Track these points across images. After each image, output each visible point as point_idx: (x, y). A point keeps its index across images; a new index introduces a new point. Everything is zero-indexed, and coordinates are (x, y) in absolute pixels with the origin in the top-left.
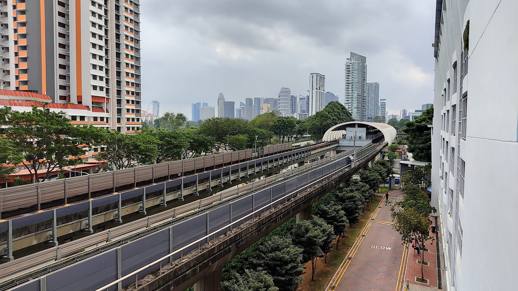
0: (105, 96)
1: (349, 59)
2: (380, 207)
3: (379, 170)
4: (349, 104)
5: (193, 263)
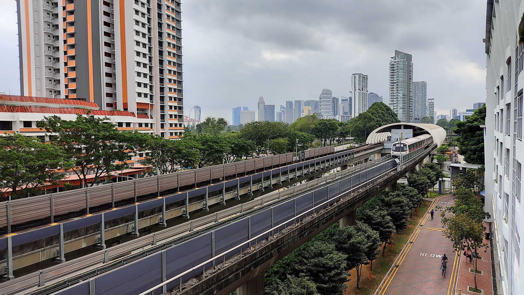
0: (149, 103)
1: (393, 58)
3: (427, 174)
4: (394, 105)
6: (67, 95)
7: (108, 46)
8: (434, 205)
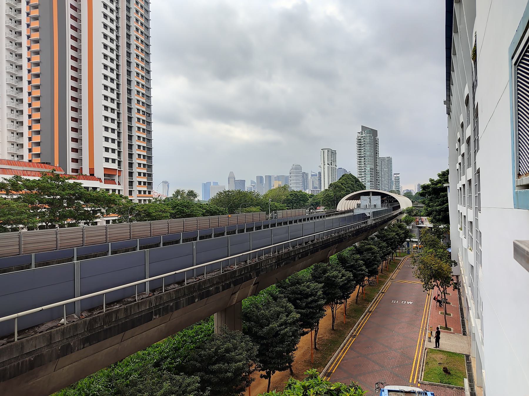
1: (360, 133)
3: (396, 231)
4: (362, 178)
6: (31, 159)
7: (75, 110)
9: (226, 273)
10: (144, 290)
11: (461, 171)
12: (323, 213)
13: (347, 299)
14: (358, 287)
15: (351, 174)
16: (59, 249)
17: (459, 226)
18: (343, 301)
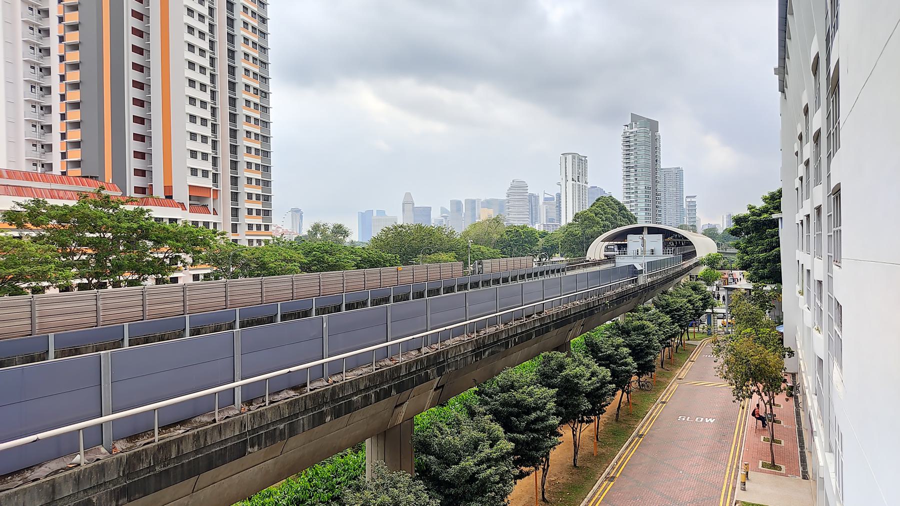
0: (211, 186)
1: (628, 126)
2: (692, 360)
3: (688, 296)
5: (364, 384)
8: (700, 350)
9: (382, 370)
10: (232, 403)
11: (805, 190)
12: (561, 263)
13: (601, 415)
14: (620, 392)
15: (611, 196)
16: (147, 319)
17: (798, 288)
18: (593, 418)
